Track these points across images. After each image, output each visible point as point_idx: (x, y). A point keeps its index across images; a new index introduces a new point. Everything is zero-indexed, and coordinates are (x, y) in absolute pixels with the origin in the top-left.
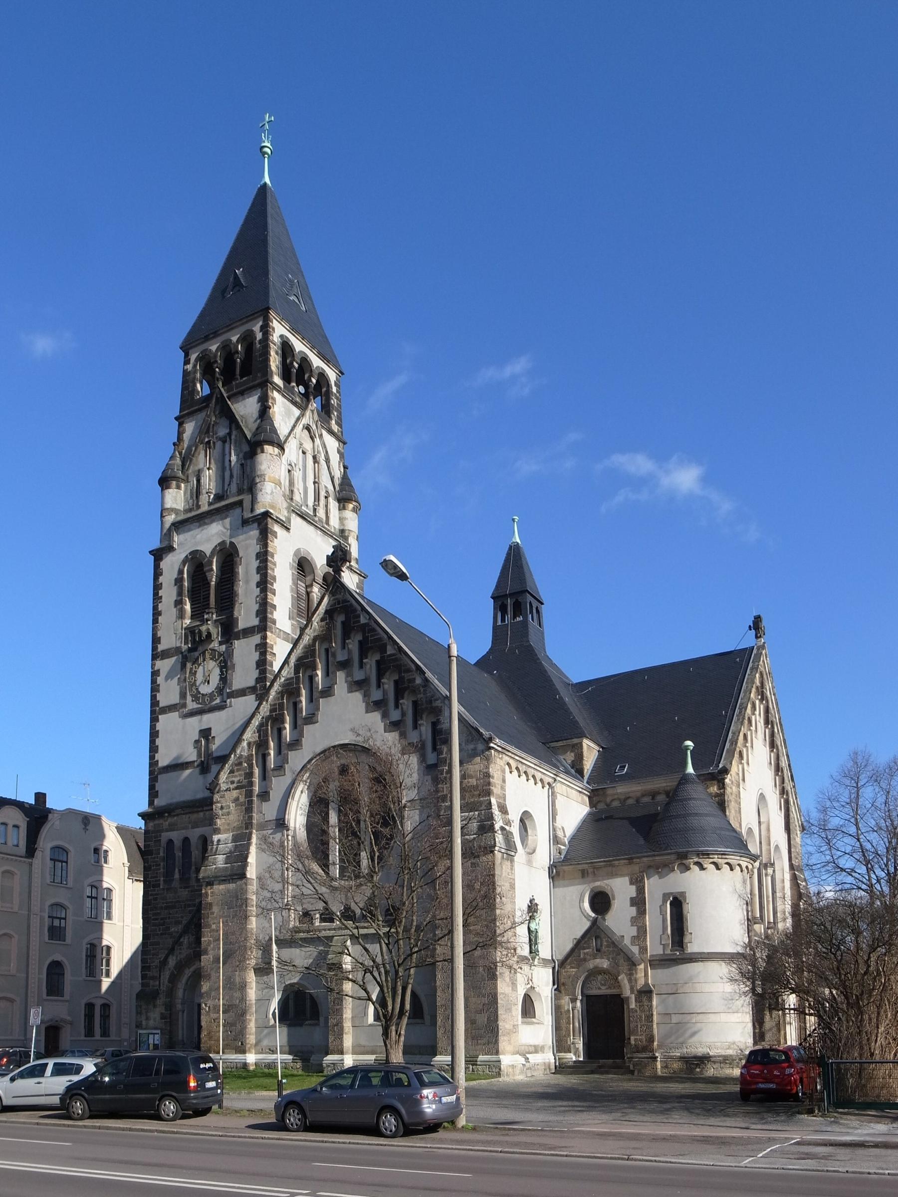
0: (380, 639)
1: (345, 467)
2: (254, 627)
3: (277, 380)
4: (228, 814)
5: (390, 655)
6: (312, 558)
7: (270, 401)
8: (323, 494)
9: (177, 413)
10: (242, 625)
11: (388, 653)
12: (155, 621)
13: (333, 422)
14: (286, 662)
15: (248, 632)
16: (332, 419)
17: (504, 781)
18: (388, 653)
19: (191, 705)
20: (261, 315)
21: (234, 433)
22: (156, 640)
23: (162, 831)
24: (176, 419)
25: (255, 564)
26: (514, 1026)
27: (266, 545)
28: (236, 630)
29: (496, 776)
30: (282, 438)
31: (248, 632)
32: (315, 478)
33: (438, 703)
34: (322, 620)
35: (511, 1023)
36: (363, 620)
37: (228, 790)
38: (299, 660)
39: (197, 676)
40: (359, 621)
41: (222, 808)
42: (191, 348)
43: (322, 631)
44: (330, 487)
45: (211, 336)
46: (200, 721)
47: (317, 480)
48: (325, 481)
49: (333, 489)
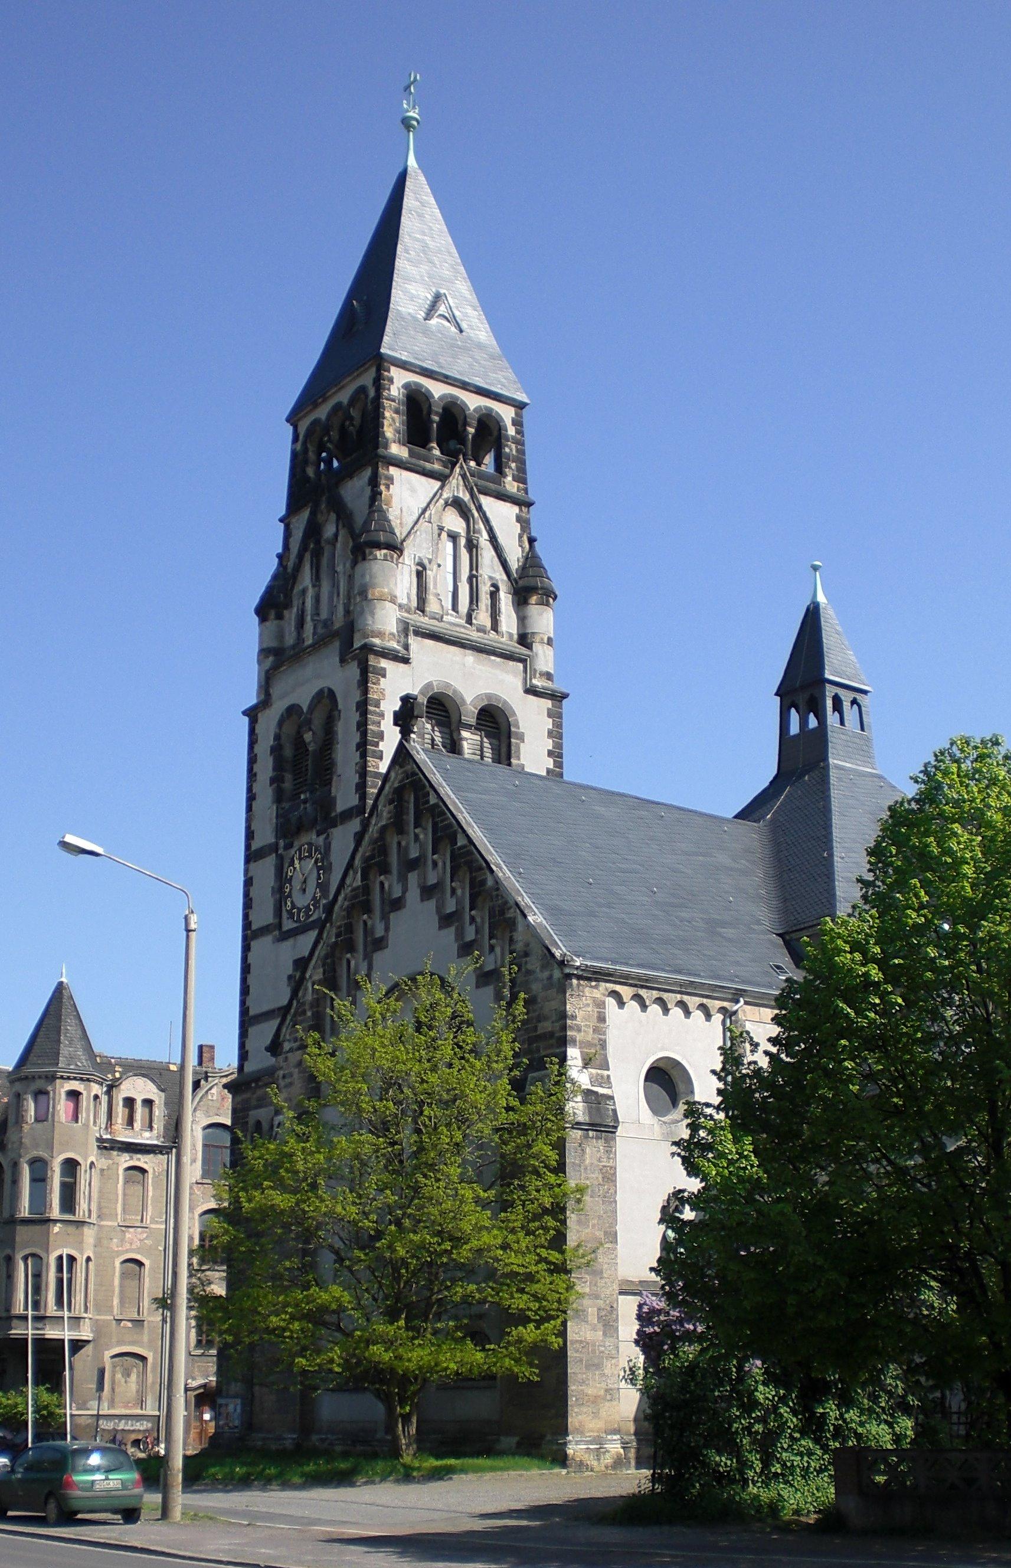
0: (450, 825)
1: (532, 541)
2: (352, 809)
3: (398, 450)
4: (291, 1084)
5: (460, 848)
6: (455, 691)
7: (383, 482)
8: (485, 589)
9: (283, 512)
10: (340, 807)
11: (459, 844)
12: (249, 809)
13: (510, 478)
14: (350, 865)
15: (347, 815)
16: (505, 476)
17: (602, 1019)
18: (459, 844)
19: (288, 925)
20: (371, 366)
21: (342, 533)
22: (250, 835)
23: (249, 1109)
24: (281, 520)
25: (356, 717)
26: (606, 1390)
27: (365, 691)
28: (333, 814)
29: (580, 1014)
30: (400, 532)
31: (347, 815)
32: (471, 569)
33: (510, 914)
34: (391, 802)
35: (603, 1385)
36: (433, 800)
37: (291, 1050)
38: (366, 860)
39: (293, 883)
40: (428, 802)
41: (284, 1077)
42: (299, 420)
43: (390, 818)
44: (501, 576)
45: (320, 400)
46: (294, 947)
47: (474, 572)
48: (490, 568)
49: (505, 577)
